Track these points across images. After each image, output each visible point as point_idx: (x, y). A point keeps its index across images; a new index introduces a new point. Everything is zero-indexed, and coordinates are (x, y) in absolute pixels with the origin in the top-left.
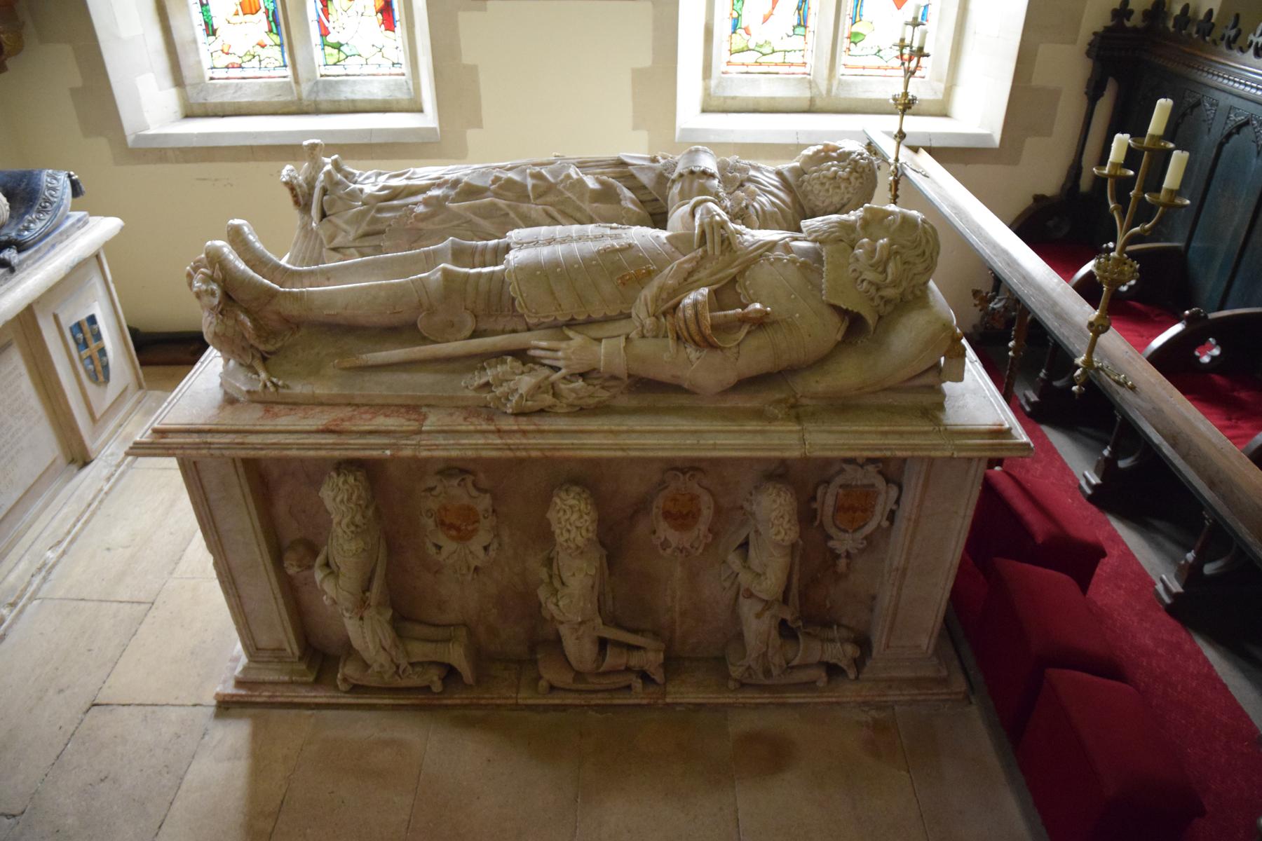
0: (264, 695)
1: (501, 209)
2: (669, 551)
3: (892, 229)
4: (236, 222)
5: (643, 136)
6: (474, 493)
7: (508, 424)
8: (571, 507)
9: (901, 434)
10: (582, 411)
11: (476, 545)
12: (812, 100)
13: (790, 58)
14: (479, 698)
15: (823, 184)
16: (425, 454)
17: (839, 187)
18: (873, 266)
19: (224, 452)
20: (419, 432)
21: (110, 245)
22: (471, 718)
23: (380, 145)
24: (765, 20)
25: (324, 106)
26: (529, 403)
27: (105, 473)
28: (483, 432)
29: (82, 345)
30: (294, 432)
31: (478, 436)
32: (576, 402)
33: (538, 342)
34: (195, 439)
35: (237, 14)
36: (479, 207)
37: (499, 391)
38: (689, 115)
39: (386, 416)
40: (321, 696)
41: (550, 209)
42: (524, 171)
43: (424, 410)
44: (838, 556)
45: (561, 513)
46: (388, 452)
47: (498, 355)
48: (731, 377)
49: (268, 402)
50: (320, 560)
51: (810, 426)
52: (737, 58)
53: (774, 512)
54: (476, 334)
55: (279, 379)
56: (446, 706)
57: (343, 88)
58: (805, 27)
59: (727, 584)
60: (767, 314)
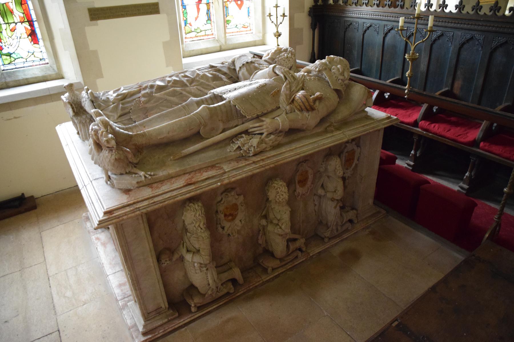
0: (161, 332)
5: (170, 68)
6: (237, 197)
7: (255, 159)
8: (281, 185)
9: (367, 125)
10: (275, 147)
11: (237, 221)
12: (220, 46)
13: (208, 32)
14: (249, 287)
15: (284, 60)
16: (233, 179)
18: (112, 150)
22: (250, 295)
24: (196, 19)
25: (11, 84)
26: (258, 149)
28: (248, 165)
30: (172, 190)
31: (248, 166)
34: (145, 203)
36: (169, 92)
37: (245, 148)
40: (186, 319)
41: (199, 87)
43: (217, 165)
46: (219, 184)
47: (237, 136)
48: (318, 120)
52: (188, 35)
54: (224, 131)
55: (151, 172)
56: (238, 297)
57: (18, 74)
58: (211, 20)
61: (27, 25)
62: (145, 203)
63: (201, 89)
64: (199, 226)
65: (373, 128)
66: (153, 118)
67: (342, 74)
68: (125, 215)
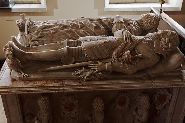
1: (73, 31)
2: (119, 111)
3: (169, 35)
6: (74, 100)
7: (85, 83)
8: (99, 102)
9: (174, 82)
10: (100, 80)
11: (73, 112)
15: (147, 24)
17: (151, 24)
19: (15, 93)
20: (64, 86)
23: (33, 13)
31: (78, 86)
32: (100, 78)
33: (91, 64)
34: (16, 90)
38: (107, 5)
39: (55, 83)
42: (77, 22)
43: (63, 81)
44: (157, 111)
45: (96, 104)
47: (80, 67)
48: (135, 70)
49: (24, 80)
50: (36, 118)
51: (154, 81)
53: (144, 101)
59: (132, 118)
60: (143, 56)
62: (16, 90)
63: (86, 32)
64: (43, 109)
65: (178, 85)
66: (42, 46)
67: (167, 44)
68: (4, 92)
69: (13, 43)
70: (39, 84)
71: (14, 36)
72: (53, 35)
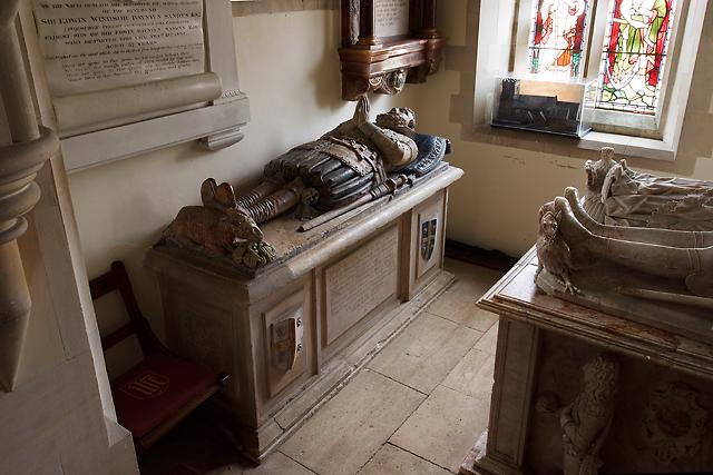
4: (572, 188)
20: (675, 351)
21: (454, 185)
27: (413, 309)
29: (425, 235)
30: (582, 323)
35: (553, 65)
43: (677, 337)
49: (567, 302)
50: (566, 410)
61: (652, 59)
69: (567, 203)
70: (604, 322)
71: (572, 188)
72: (680, 215)
